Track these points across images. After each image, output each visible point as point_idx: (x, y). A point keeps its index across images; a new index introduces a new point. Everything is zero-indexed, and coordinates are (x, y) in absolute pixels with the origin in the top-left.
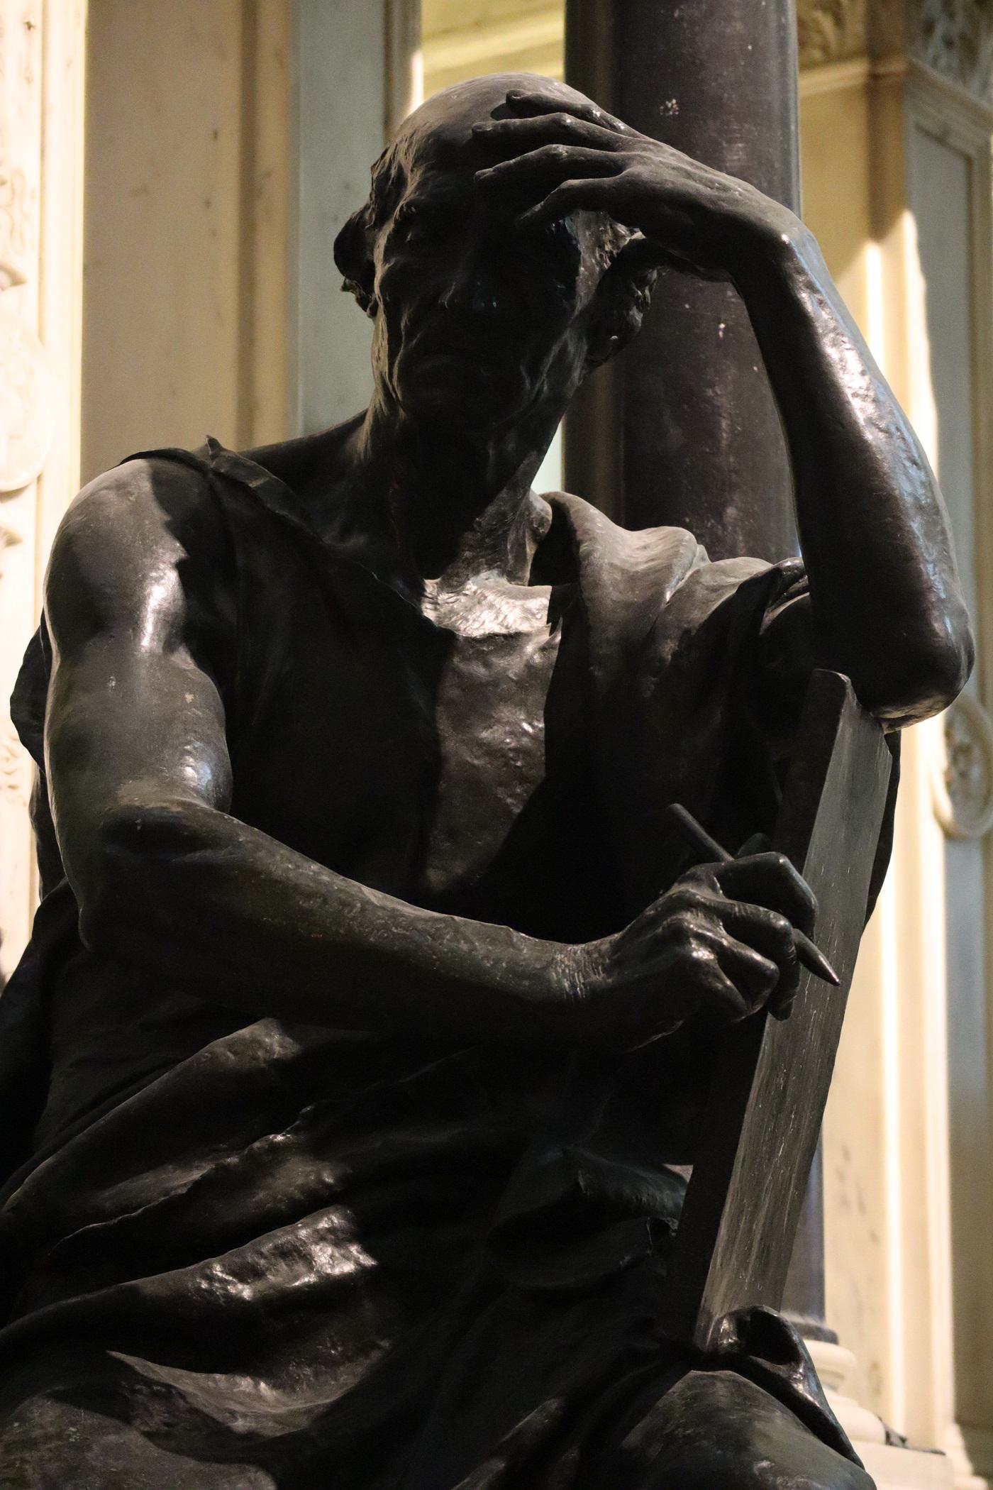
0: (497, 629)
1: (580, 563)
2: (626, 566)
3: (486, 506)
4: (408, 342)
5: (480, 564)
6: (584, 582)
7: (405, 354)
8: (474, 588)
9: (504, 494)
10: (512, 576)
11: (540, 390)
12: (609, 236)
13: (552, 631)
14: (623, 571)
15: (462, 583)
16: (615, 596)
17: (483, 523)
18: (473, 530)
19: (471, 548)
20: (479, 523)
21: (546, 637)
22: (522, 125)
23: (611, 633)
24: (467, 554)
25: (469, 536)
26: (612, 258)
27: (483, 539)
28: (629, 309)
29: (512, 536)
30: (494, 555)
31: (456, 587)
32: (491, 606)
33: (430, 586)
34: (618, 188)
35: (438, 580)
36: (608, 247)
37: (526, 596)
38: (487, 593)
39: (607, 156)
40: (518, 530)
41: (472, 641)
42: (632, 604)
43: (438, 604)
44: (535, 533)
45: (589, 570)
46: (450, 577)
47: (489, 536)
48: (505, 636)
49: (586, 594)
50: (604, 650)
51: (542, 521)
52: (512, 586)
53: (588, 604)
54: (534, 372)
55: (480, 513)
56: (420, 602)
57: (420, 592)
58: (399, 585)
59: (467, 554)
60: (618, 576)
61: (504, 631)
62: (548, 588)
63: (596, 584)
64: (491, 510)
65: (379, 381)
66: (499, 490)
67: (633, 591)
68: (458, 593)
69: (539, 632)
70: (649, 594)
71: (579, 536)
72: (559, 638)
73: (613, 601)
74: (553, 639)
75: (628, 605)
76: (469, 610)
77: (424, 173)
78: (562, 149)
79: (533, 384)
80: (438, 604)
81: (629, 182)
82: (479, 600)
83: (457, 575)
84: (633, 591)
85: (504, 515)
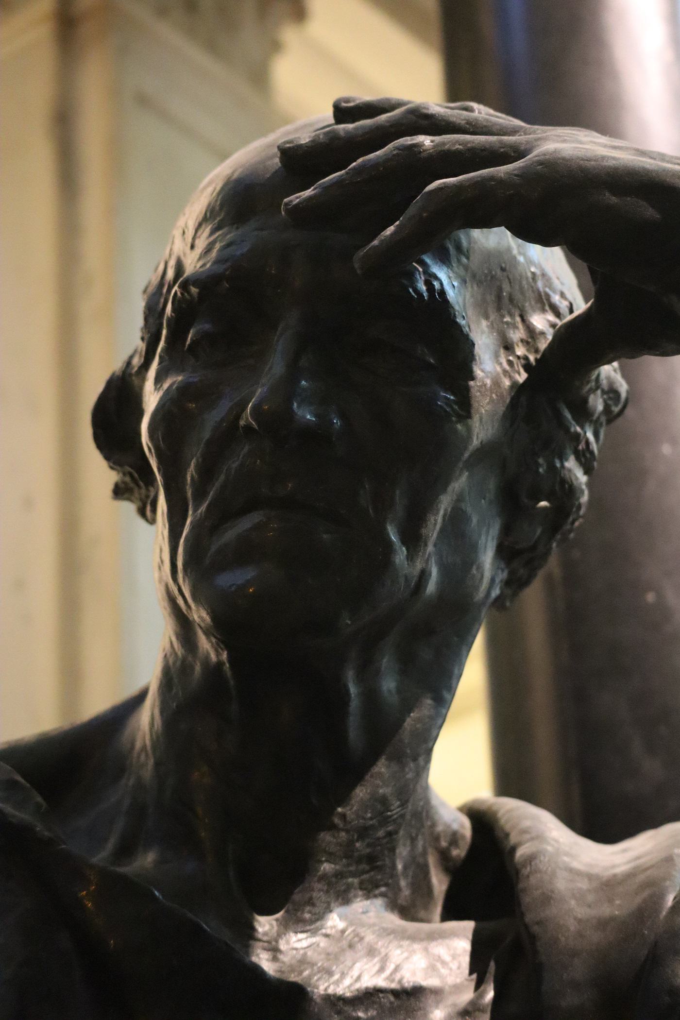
0: (381, 982)
1: (518, 872)
2: (595, 871)
3: (353, 787)
4: (195, 511)
5: (349, 887)
6: (526, 900)
7: (194, 526)
8: (341, 925)
9: (382, 767)
10: (407, 912)
11: (424, 575)
12: (517, 335)
13: (479, 984)
14: (590, 877)
15: (320, 917)
16: (581, 912)
17: (350, 814)
18: (333, 827)
19: (332, 857)
20: (343, 816)
21: (468, 995)
22: (356, 129)
23: (579, 970)
24: (327, 867)
25: (326, 838)
26: (527, 367)
27: (351, 843)
28: (562, 458)
29: (403, 851)
30: (370, 870)
31: (312, 922)
32: (371, 952)
33: (265, 925)
34: (525, 176)
35: (279, 915)
36: (520, 351)
37: (432, 937)
38: (362, 931)
39: (501, 142)
40: (413, 840)
41: (335, 1002)
42: (613, 919)
43: (284, 948)
44: (444, 856)
45: (533, 880)
46: (299, 907)
47: (361, 837)
48: (395, 993)
49: (529, 918)
50: (570, 1000)
51: (455, 838)
52: (412, 926)
53: (536, 929)
54: (413, 539)
55: (343, 798)
56: (247, 949)
57: (248, 934)
58: (211, 926)
59: (327, 867)
60: (584, 885)
61: (394, 986)
62: (469, 926)
63: (547, 899)
64: (361, 793)
65: (165, 603)
66: (373, 761)
67: (611, 901)
68: (314, 932)
69: (457, 989)
70: (638, 900)
71: (513, 839)
72: (490, 995)
73: (580, 921)
74: (481, 996)
75: (602, 924)
76: (334, 957)
77: (212, 233)
78: (426, 141)
79: (411, 557)
80: (284, 948)
81: (540, 163)
82: (349, 944)
83: (310, 902)
84: (611, 901)
85: (384, 801)
